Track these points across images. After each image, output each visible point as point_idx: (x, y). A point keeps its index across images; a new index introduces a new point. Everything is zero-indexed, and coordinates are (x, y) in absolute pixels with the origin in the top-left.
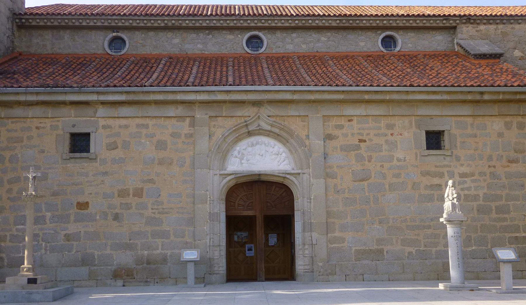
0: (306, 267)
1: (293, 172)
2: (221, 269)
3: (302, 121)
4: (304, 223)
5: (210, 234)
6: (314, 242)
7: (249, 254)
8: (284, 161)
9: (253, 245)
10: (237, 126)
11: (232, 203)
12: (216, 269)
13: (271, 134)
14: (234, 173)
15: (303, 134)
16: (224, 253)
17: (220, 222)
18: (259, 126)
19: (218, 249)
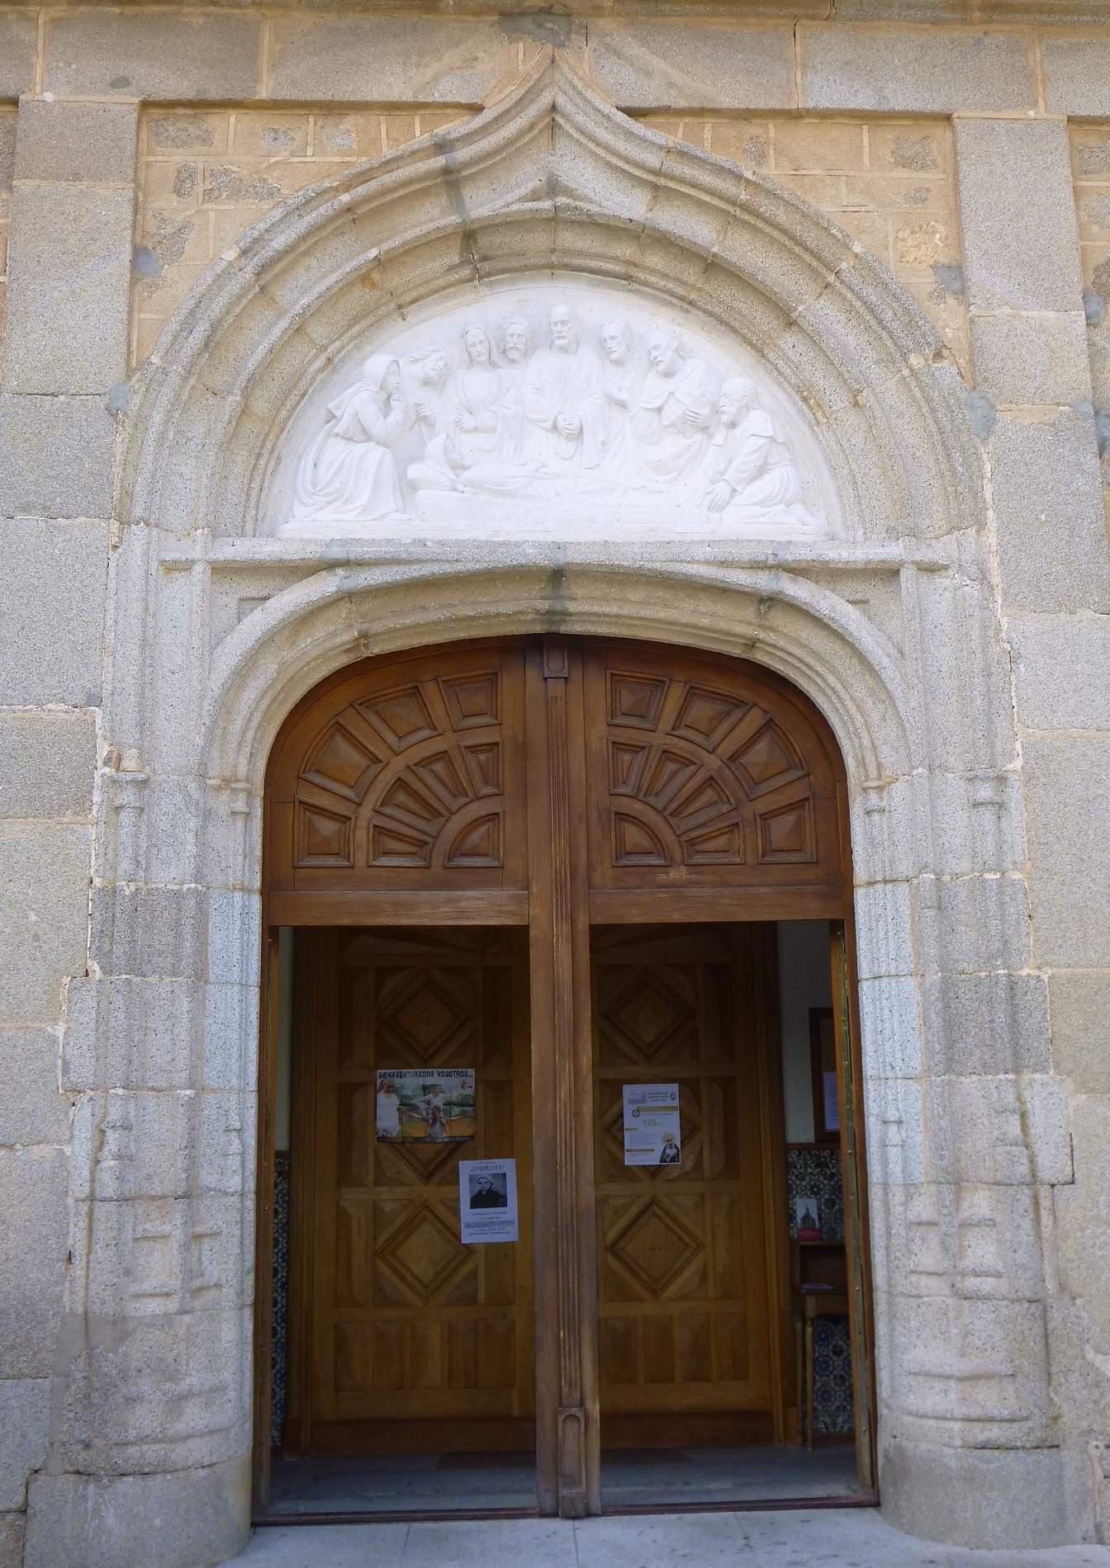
0: (989, 1399)
1: (838, 554)
2: (194, 1416)
3: (906, 163)
4: (947, 988)
5: (102, 1086)
6: (1051, 1163)
7: (479, 1228)
8: (762, 470)
9: (508, 1166)
10: (365, 176)
11: (327, 827)
12: (144, 1419)
13: (655, 260)
14: (337, 553)
15: (913, 257)
16: (230, 1260)
17: (200, 975)
18: (553, 187)
19: (174, 1226)
